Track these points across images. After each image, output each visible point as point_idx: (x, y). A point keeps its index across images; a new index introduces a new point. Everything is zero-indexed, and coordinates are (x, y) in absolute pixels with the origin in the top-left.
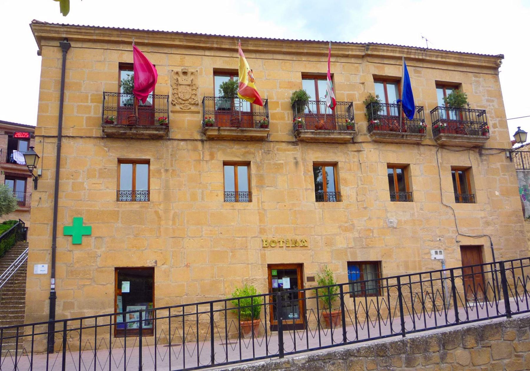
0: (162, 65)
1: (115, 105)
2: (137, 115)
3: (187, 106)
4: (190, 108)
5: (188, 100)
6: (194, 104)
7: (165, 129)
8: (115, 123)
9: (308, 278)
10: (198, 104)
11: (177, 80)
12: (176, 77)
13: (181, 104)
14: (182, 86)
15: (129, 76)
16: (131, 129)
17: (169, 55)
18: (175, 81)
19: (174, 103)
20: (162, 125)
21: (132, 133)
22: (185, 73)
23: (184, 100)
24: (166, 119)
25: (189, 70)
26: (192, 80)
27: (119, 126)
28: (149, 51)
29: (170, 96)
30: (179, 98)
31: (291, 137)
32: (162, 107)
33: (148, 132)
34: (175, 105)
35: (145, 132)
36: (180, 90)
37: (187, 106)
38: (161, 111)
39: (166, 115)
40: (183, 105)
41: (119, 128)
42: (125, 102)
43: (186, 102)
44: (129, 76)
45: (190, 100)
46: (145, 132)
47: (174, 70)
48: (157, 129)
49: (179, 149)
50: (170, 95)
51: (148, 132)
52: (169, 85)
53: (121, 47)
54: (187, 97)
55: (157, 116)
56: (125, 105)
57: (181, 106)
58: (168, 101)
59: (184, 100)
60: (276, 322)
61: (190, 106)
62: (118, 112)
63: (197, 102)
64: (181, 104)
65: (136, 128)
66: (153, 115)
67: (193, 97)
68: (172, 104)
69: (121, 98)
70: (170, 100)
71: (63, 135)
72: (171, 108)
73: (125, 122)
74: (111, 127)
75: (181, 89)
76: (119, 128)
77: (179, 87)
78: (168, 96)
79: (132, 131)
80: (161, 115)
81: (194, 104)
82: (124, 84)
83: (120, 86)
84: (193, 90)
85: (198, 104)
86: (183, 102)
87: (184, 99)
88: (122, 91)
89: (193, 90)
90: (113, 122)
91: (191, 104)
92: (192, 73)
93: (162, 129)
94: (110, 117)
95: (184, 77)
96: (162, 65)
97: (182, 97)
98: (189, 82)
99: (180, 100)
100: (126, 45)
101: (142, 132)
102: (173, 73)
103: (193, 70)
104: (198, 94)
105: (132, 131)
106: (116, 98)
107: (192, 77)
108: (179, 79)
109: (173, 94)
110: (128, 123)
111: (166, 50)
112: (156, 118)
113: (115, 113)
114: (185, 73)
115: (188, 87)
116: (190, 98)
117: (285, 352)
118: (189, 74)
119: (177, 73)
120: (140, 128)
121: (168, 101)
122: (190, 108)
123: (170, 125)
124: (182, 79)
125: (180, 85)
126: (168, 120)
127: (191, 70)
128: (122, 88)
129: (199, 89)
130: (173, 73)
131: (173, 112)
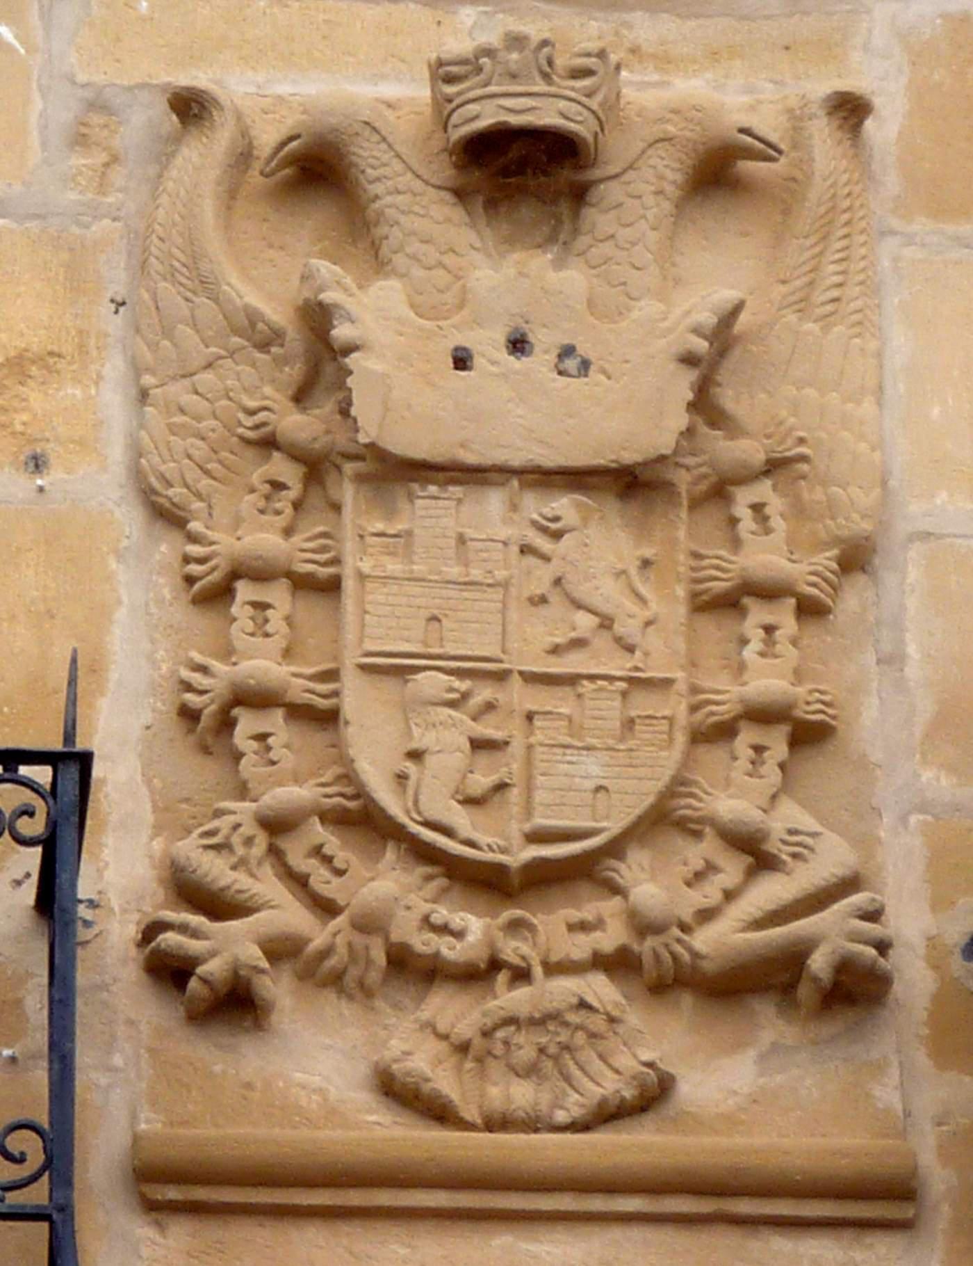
3: (559, 1038)
4: (653, 1095)
5: (577, 872)
6: (764, 981)
10: (855, 991)
11: (321, 355)
12: (270, 270)
13: (412, 970)
14: (433, 513)
18: (262, 389)
19: (224, 948)
22: (523, 170)
23: (485, 882)
25: (642, 91)
26: (712, 359)
29: (118, 780)
30: (365, 821)
31: (562, 955)
34: (237, 1005)
36: (380, 617)
37: (559, 1038)
40: (456, 1011)
43: (554, 927)
45: (650, 883)
50: (124, 740)
52: (96, 484)
54: (583, 783)
57: (413, 1037)
58: (52, 900)
59: (485, 882)
61: (657, 1038)
63: (831, 935)
64: (412, 970)
67: (735, 792)
68: (170, 972)
71: (61, 766)
75: (415, 578)
77: (361, 532)
78: (75, 764)
81: (764, 981)
84: (727, 603)
85: (855, 991)
86: (474, 929)
87: (499, 840)
89: (727, 603)
91: (657, 972)
92: (718, 173)
95: (504, 274)
97: (430, 799)
98: (632, 412)
99: (385, 885)
102: (203, 158)
103: (741, 97)
104: (881, 722)
107: (720, 270)
108: (373, 313)
109: (209, 723)
114: (523, 170)
115: (602, 548)
116: (663, 819)
117: (39, 849)
118: (636, 194)
119: (317, 171)
121: (52, 900)
122: (653, 1095)
124: (435, 324)
125: (397, 473)
127: (675, 84)
129: (907, 580)
130: (203, 158)
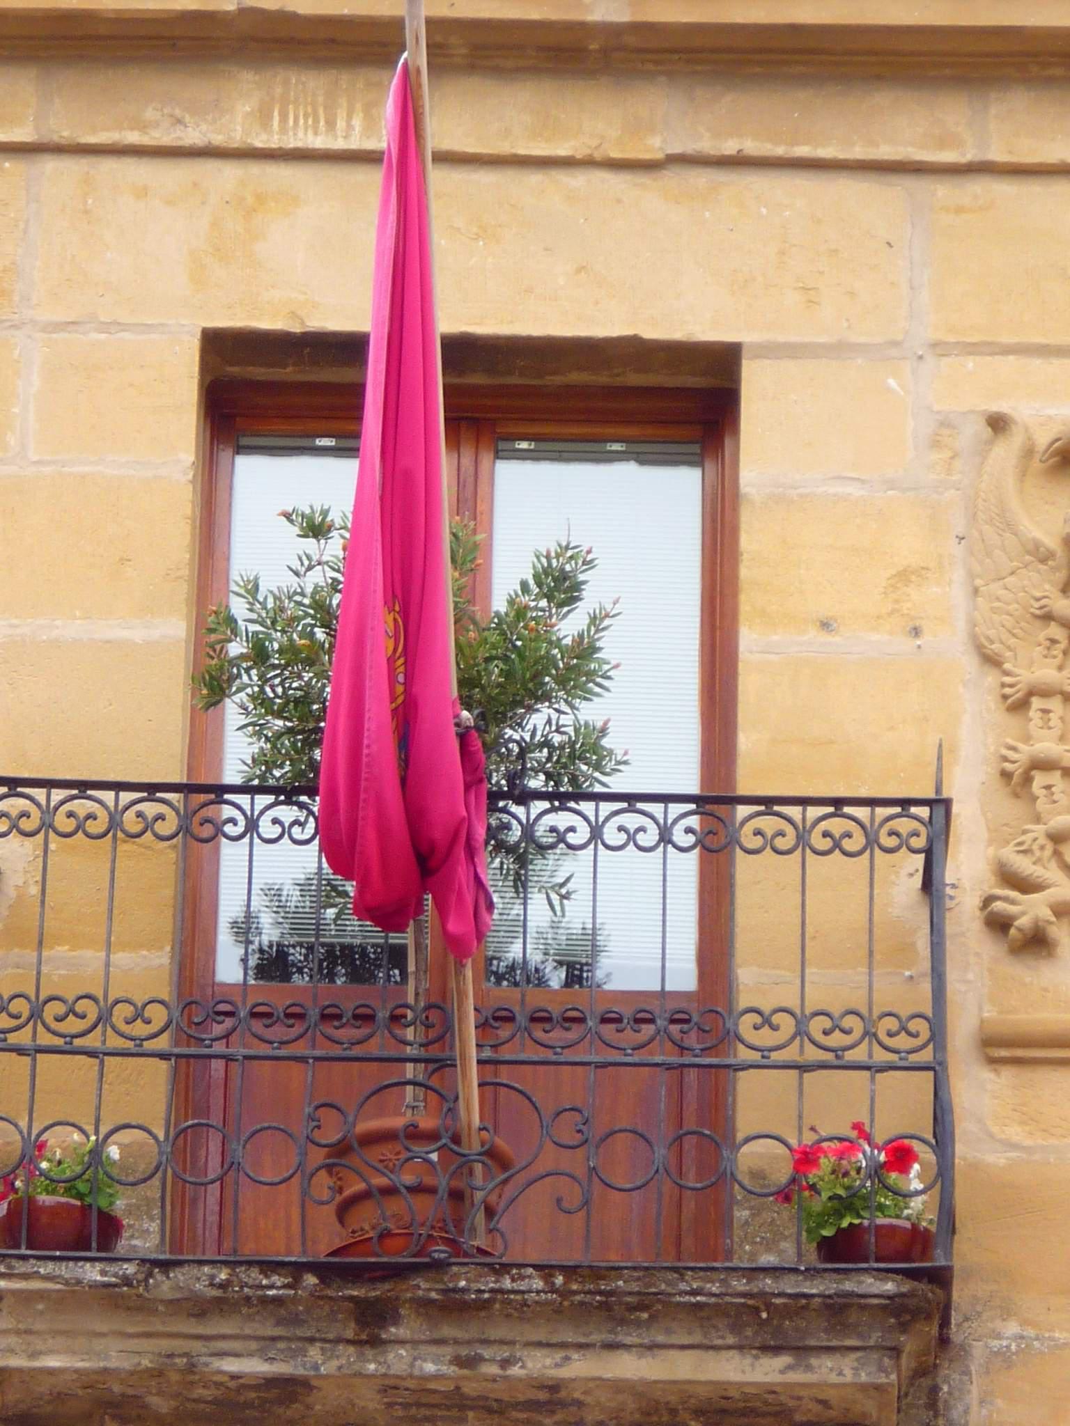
0: (839, 350)
1: (145, 968)
2: (472, 1110)
7: (899, 1311)
8: (143, 1236)
9: (433, 153)
15: (316, 529)
16: (372, 1323)
17: (943, 190)
19: (1029, 910)
20: (842, 1249)
21: (388, 1387)
24: (901, 1157)
27: (197, 1280)
28: (654, 146)
29: (965, 814)
32: (834, 986)
33: (629, 1367)
35: (580, 1367)
38: (825, 1046)
39: (899, 1106)
41: (200, 1308)
42: (269, 932)
44: (316, 529)
46: (580, 1367)
47: (1021, 409)
48: (765, 1323)
49: (543, 849)
51: (629, 1367)
52: (949, 642)
53: (241, 107)
55: (769, 1117)
56: (273, 965)
60: (487, 1053)
62: (187, 1068)
65: (454, 1307)
66: (704, 1124)
68: (999, 925)
69: (232, 856)
70: (968, 869)
72: (982, 987)
73: (290, 1217)
74: (75, 1297)
76: (200, 1308)
78: (940, 805)
79: (398, 1360)
80: (836, 1105)
82: (259, 654)
83: (212, 685)
88: (238, 754)
90: (110, 1228)
93: (838, 1310)
94: (65, 1144)
96: (839, 350)
100: (310, 84)
101: (538, 1364)
102: (1005, 452)
105: (398, 1360)
106: (151, 869)
109: (1018, 780)
110: (327, 1237)
111: (905, 125)
112: (760, 1158)
113: (144, 1091)
120: (521, 1309)
121: (929, 883)
123: (966, 1253)
126: (944, 1175)
128: (233, 712)
131: (1007, 1049)
